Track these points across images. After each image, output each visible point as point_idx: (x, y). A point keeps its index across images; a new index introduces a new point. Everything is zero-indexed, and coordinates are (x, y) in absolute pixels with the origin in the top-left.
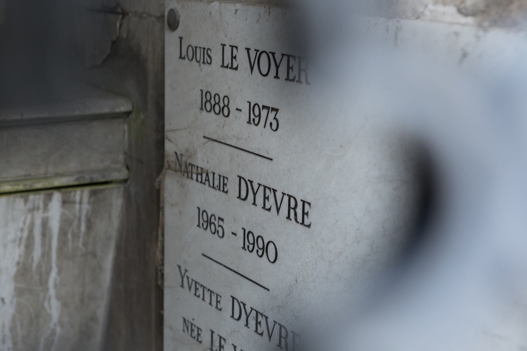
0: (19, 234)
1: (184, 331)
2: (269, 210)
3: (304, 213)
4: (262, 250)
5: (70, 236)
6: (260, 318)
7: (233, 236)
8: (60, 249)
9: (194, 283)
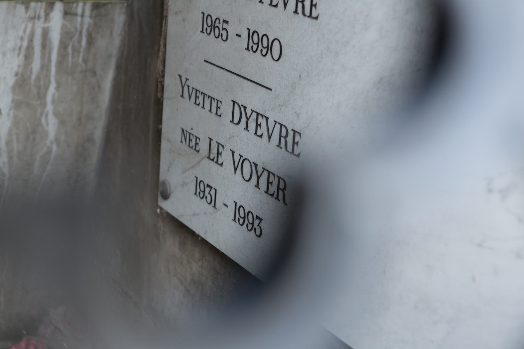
0: (19, 43)
1: (181, 142)
2: (276, 6)
3: (312, 5)
4: (266, 49)
5: (70, 50)
6: (260, 120)
7: (238, 37)
8: (60, 63)
9: (194, 91)
